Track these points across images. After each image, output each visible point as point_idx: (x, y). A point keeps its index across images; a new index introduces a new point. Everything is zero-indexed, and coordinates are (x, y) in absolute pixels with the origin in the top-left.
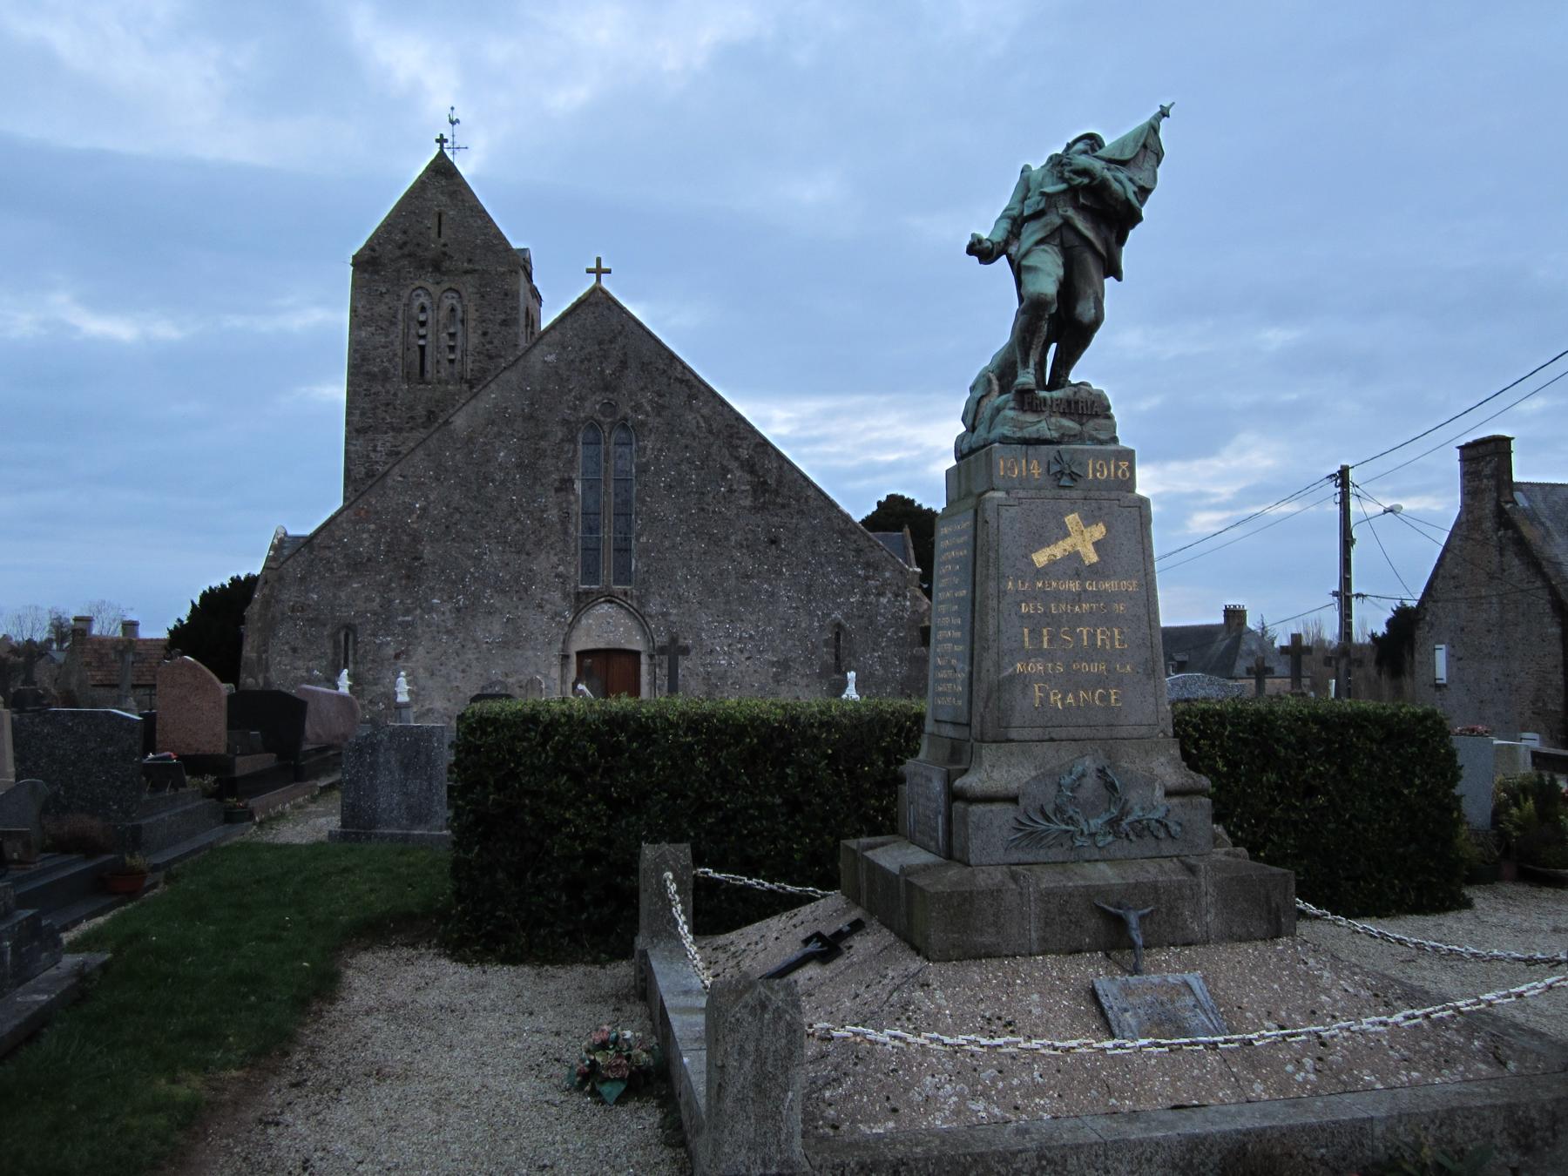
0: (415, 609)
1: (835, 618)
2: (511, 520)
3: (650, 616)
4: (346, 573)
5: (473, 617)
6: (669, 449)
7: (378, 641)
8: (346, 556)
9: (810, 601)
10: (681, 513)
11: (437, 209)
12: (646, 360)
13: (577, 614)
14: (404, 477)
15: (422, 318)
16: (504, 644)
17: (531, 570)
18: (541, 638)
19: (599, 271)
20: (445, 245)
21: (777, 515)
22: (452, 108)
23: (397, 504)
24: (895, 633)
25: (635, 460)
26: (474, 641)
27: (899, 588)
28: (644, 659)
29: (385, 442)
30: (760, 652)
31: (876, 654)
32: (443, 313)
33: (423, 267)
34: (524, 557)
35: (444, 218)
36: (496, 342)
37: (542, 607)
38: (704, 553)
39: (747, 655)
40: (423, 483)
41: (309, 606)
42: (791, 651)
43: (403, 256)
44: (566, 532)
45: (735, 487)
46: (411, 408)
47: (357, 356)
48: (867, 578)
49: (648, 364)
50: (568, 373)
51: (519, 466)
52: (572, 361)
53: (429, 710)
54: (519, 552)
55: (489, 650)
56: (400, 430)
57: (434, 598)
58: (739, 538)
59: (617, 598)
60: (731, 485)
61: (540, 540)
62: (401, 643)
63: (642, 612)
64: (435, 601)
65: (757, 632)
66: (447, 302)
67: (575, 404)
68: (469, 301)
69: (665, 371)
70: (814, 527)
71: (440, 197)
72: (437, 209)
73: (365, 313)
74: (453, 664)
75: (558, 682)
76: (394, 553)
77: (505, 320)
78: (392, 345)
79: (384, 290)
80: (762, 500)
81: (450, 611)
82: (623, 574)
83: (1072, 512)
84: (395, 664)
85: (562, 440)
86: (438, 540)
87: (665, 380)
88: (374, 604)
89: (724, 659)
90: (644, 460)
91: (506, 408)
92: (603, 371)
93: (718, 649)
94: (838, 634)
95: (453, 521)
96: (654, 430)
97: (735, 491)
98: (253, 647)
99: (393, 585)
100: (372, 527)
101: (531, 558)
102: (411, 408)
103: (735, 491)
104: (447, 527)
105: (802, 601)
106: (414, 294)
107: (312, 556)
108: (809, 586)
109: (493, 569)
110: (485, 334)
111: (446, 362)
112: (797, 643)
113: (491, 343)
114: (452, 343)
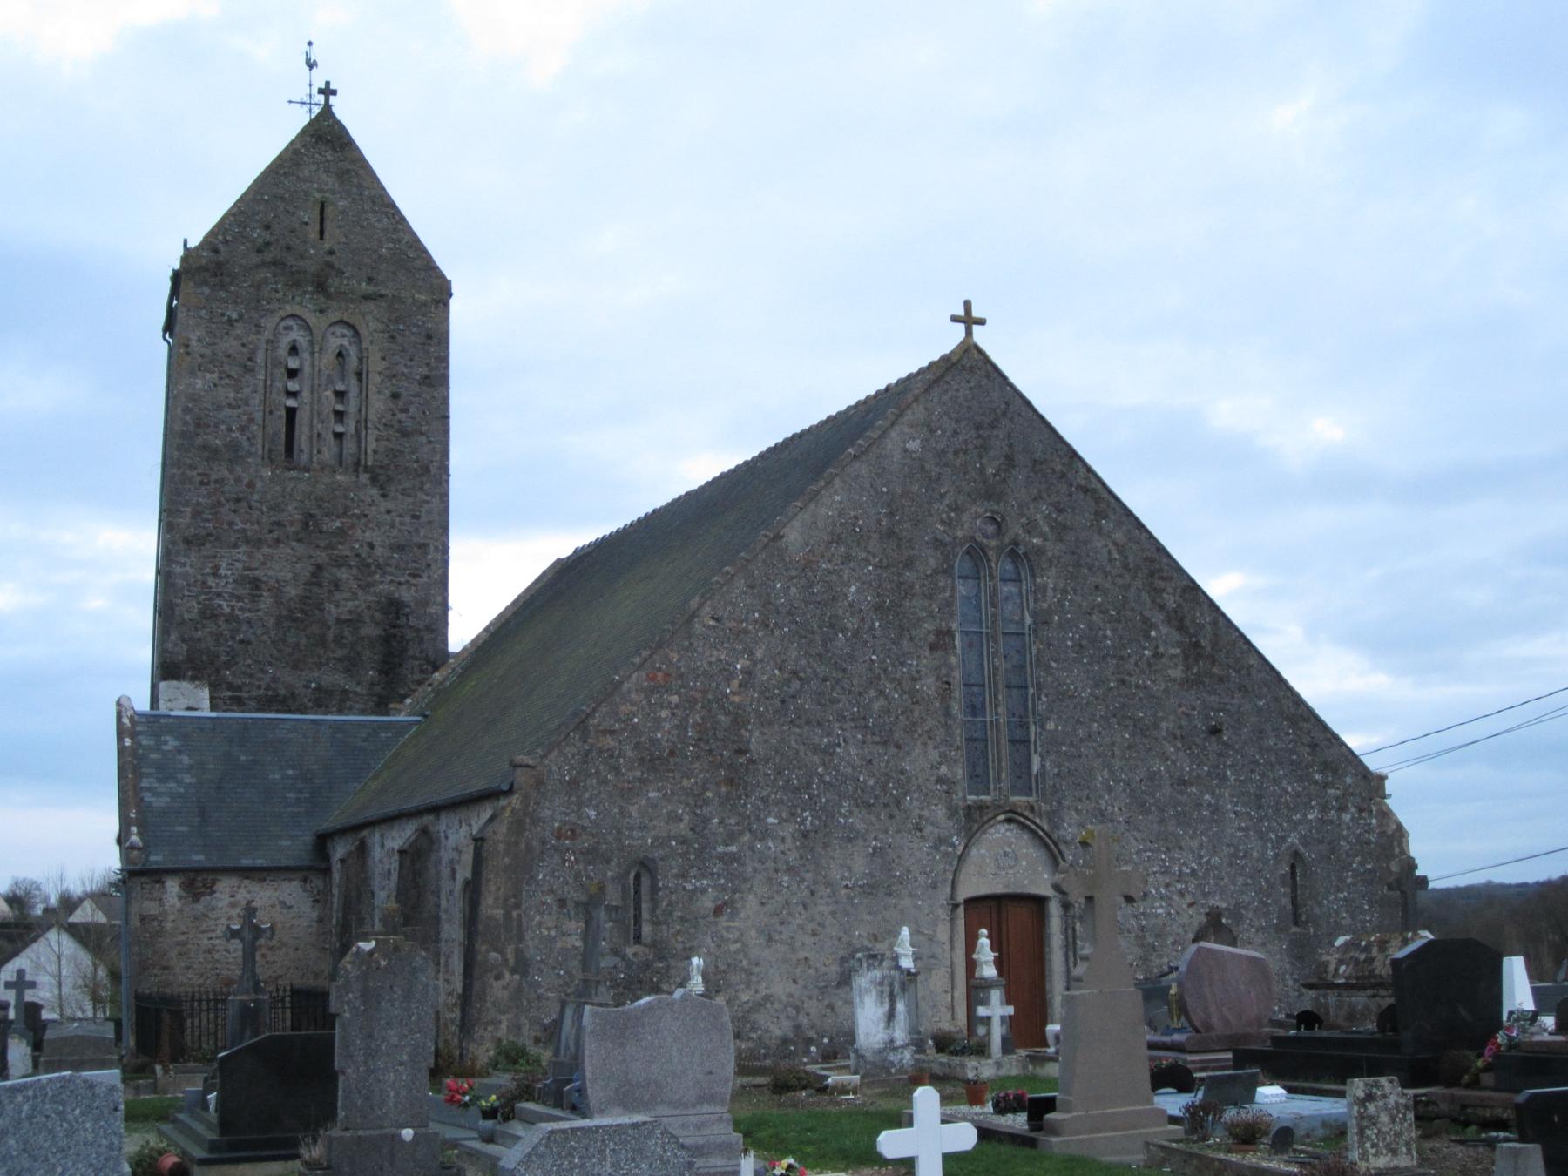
0: (741, 833)
1: (1292, 844)
2: (872, 693)
3: (1066, 842)
4: (639, 774)
5: (825, 846)
6: (1075, 591)
7: (689, 887)
8: (637, 746)
9: (1261, 819)
10: (1097, 686)
11: (318, 195)
12: (1037, 456)
13: (969, 840)
14: (717, 620)
15: (293, 363)
16: (870, 889)
17: (902, 772)
18: (922, 879)
19: (968, 320)
20: (331, 253)
21: (1215, 693)
22: (310, 44)
23: (710, 663)
24: (1362, 864)
25: (1032, 605)
26: (828, 884)
27: (1363, 799)
28: (1054, 909)
29: (232, 562)
30: (1206, 895)
31: (1341, 896)
32: (328, 359)
33: (297, 284)
34: (893, 750)
35: (329, 210)
36: (412, 410)
37: (921, 830)
38: (1130, 747)
39: (1189, 899)
40: (746, 631)
41: (584, 828)
42: (1242, 892)
43: (264, 264)
44: (947, 713)
45: (1161, 650)
46: (276, 508)
47: (188, 418)
48: (1326, 785)
49: (1041, 463)
50: (937, 469)
51: (878, 608)
52: (943, 451)
53: (767, 998)
54: (885, 743)
55: (850, 899)
56: (258, 543)
57: (769, 815)
58: (1171, 725)
59: (1021, 815)
60: (1157, 647)
61: (914, 724)
62: (723, 889)
63: (1055, 836)
64: (771, 820)
65: (1199, 864)
66: (334, 343)
67: (949, 517)
68: (372, 342)
69: (1063, 475)
70: (1260, 711)
71: (324, 177)
72: (318, 195)
73: (203, 351)
74: (799, 921)
75: (947, 947)
76: (707, 742)
77: (427, 377)
78: (247, 404)
79: (234, 316)
80: (1195, 671)
81: (793, 836)
82: (1023, 778)
83: (132, 743)
84: (716, 923)
85: (936, 571)
86: (770, 723)
87: (1065, 487)
88: (682, 826)
89: (1161, 907)
90: (1045, 605)
91: (856, 518)
92: (982, 470)
93: (1153, 891)
94: (1293, 867)
95: (791, 691)
96: (1055, 562)
97: (1162, 655)
98: (497, 899)
99: (709, 794)
100: (675, 699)
101: (902, 754)
102: (276, 508)
103: (1162, 655)
104: (783, 702)
105: (1252, 818)
106: (283, 324)
107: (586, 747)
108: (1259, 797)
109: (850, 770)
110: (395, 396)
111: (331, 436)
112: (1250, 881)
113: (406, 411)
114: (339, 407)
